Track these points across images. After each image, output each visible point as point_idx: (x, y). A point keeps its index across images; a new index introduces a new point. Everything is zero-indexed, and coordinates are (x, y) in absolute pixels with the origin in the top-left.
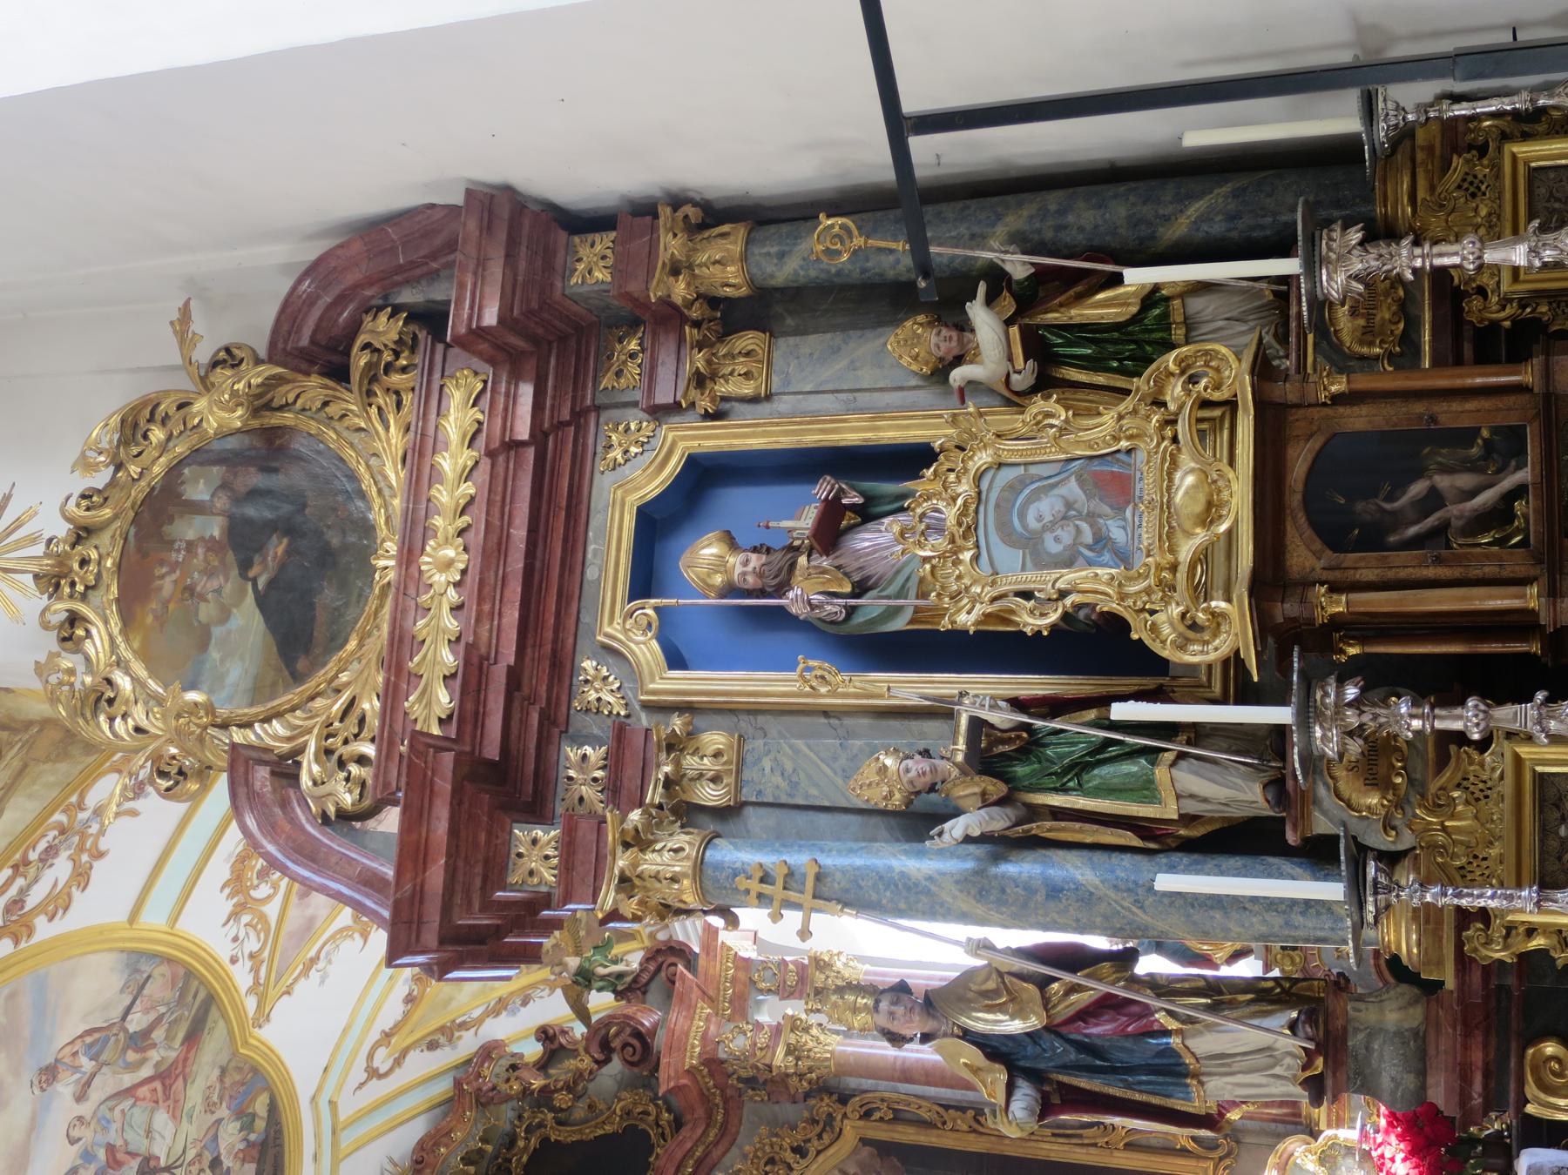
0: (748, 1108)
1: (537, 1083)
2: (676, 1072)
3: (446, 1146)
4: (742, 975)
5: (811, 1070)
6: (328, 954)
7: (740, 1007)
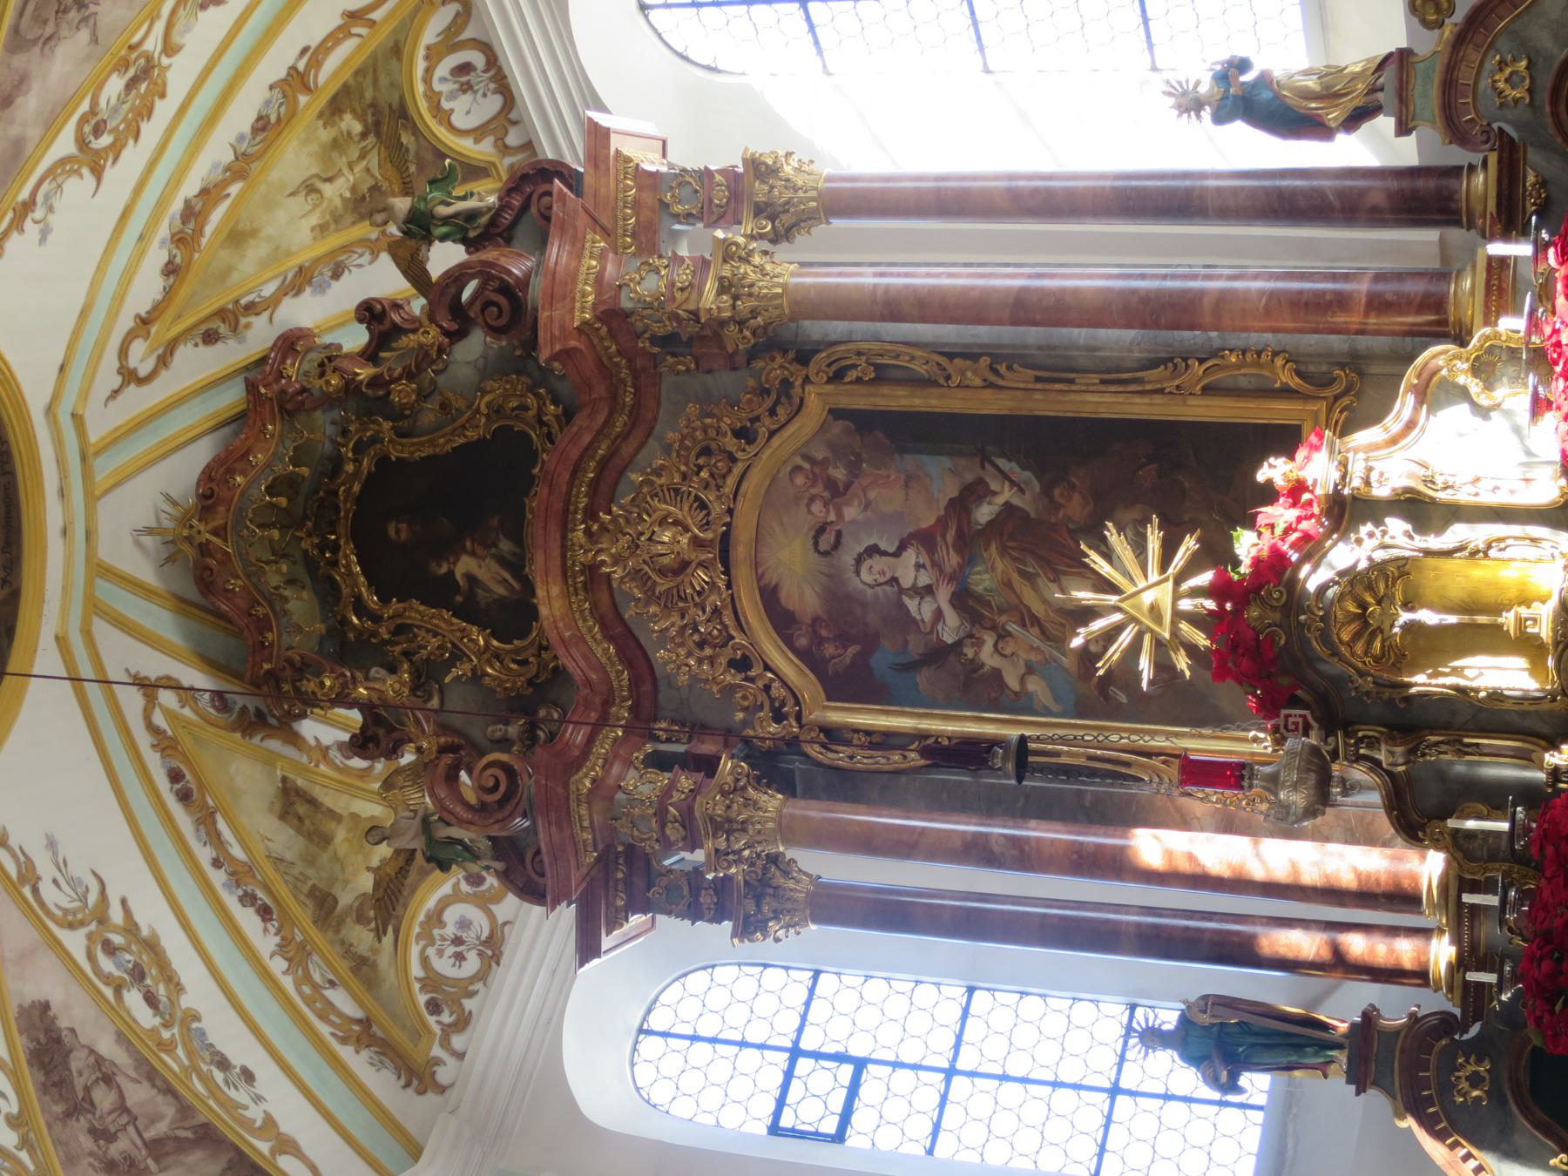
0: (668, 382)
1: (364, 373)
2: (562, 328)
3: (244, 473)
4: (648, 198)
5: (754, 313)
6: (47, 197)
7: (647, 240)
